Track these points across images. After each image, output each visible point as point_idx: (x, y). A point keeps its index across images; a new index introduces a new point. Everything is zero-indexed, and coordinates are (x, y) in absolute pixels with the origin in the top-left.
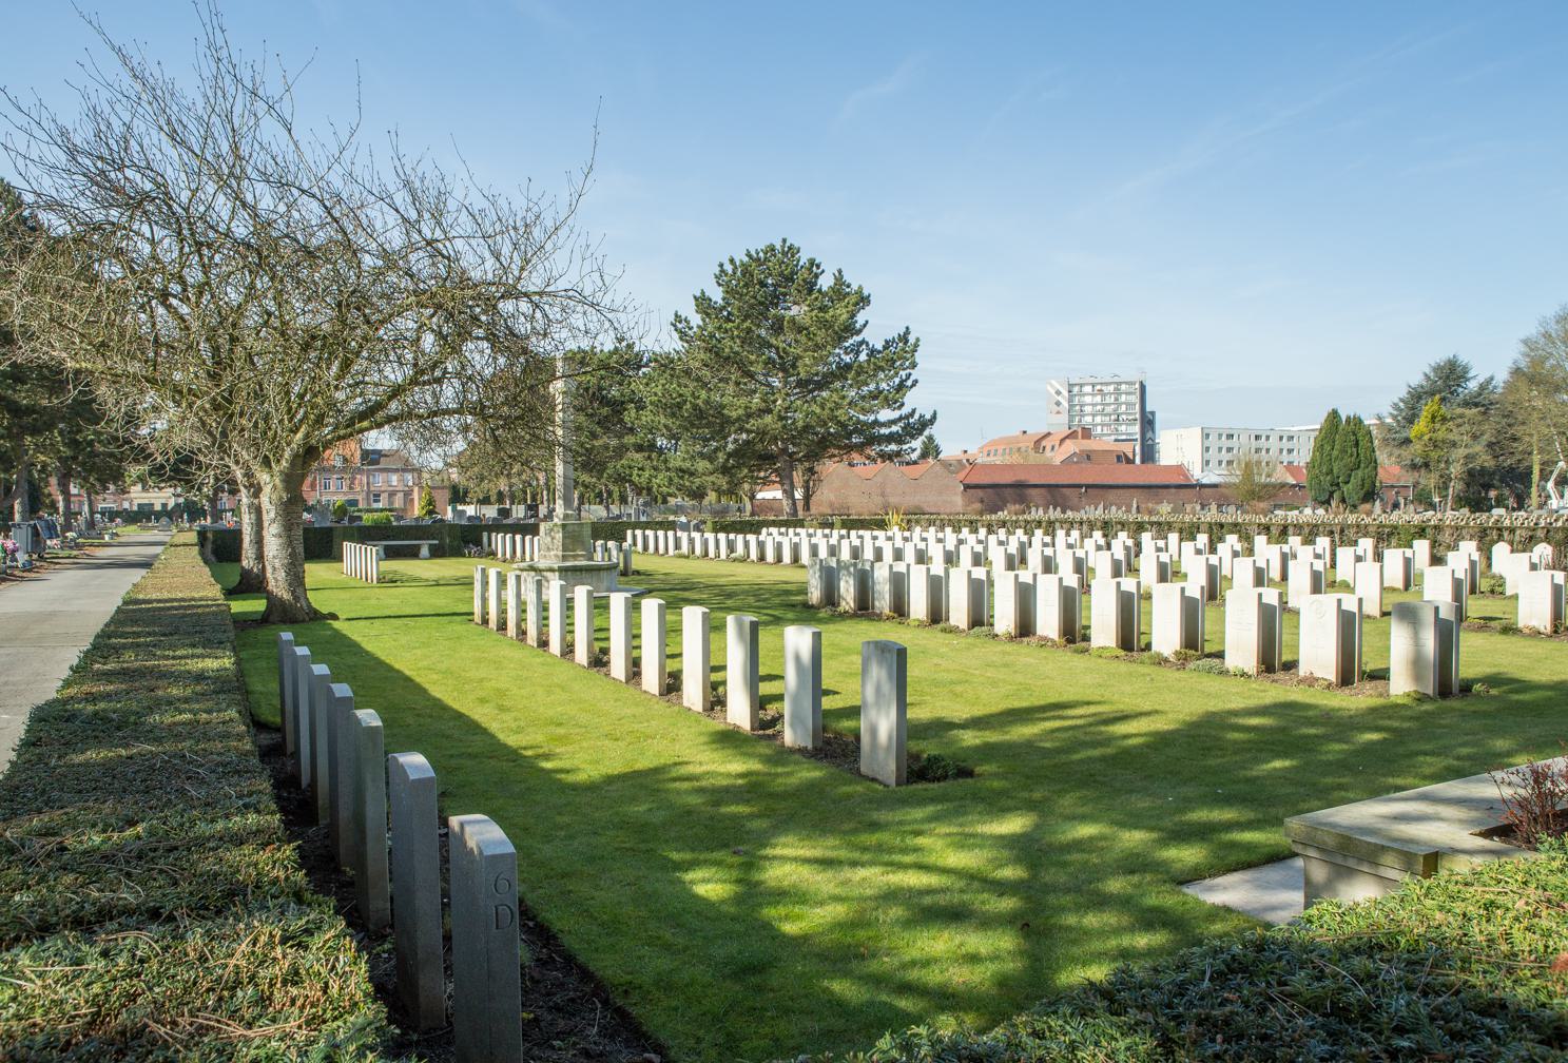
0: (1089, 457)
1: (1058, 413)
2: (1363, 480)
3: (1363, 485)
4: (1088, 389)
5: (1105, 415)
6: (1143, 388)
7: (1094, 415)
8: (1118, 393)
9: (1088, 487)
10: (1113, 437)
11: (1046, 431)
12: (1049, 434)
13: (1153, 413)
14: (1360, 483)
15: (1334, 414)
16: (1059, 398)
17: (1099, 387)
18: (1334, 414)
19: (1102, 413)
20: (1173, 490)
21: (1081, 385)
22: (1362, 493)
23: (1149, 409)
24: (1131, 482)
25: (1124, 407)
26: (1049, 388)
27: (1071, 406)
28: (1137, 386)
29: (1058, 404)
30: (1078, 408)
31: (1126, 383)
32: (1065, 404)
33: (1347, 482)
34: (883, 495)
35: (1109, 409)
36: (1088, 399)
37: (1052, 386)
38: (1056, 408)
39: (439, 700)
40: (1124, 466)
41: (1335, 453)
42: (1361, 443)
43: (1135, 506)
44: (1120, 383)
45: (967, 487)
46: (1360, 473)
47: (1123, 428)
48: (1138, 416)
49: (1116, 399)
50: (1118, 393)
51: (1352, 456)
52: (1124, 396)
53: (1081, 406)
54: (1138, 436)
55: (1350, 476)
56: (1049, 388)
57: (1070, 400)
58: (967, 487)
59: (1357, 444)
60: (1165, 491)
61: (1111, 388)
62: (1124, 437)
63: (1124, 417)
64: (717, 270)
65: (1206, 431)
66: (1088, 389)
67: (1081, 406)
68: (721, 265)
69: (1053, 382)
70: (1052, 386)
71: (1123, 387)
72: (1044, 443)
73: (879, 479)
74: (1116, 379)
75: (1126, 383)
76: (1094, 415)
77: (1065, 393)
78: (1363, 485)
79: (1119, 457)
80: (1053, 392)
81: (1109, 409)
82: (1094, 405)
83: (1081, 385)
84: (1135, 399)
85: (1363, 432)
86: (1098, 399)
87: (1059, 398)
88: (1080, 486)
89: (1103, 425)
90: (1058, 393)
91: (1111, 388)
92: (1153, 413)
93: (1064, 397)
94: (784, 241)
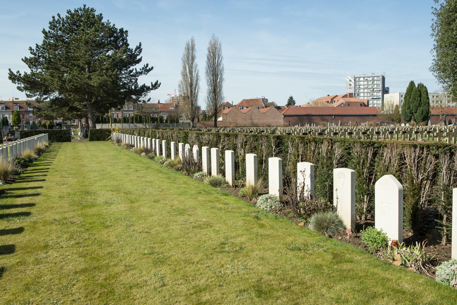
0: (349, 105)
1: (350, 88)
2: (422, 111)
3: (422, 113)
4: (362, 79)
5: (369, 89)
6: (383, 79)
7: (364, 89)
8: (373, 80)
9: (335, 116)
10: (371, 97)
11: (336, 95)
12: (337, 96)
13: (388, 88)
14: (421, 112)
15: (412, 83)
16: (351, 83)
17: (366, 78)
18: (412, 83)
19: (367, 88)
20: (371, 117)
21: (359, 78)
22: (422, 117)
23: (386, 86)
24: (353, 113)
25: (376, 86)
26: (347, 79)
27: (355, 86)
28: (381, 78)
29: (350, 85)
30: (358, 86)
31: (377, 77)
32: (353, 85)
33: (416, 113)
34: (251, 119)
35: (370, 87)
36: (362, 83)
37: (348, 78)
38: (349, 87)
39: (16, 208)
40: (363, 107)
41: (411, 100)
42: (422, 95)
43: (340, 123)
44: (374, 77)
45: (285, 116)
46: (421, 108)
47: (375, 94)
48: (381, 89)
49: (373, 83)
50: (373, 80)
51: (417, 101)
52: (376, 82)
53: (359, 86)
54: (381, 97)
55: (417, 110)
56: (347, 79)
57: (355, 84)
58: (285, 116)
59: (420, 96)
60: (368, 117)
61: (371, 79)
62: (375, 97)
63: (376, 89)
64: (51, 20)
65: (401, 94)
66: (362, 79)
67: (359, 86)
68: (54, 17)
69: (348, 77)
70: (348, 78)
71: (376, 78)
72: (335, 99)
73: (249, 113)
74: (373, 75)
75: (377, 77)
76: (364, 89)
77: (353, 81)
78: (422, 113)
79: (361, 105)
80: (348, 80)
81: (370, 87)
82: (364, 85)
83: (359, 78)
84: (380, 83)
85: (423, 90)
86: (366, 83)
87: (351, 83)
88: (332, 115)
89: (367, 93)
90: (350, 81)
91: (371, 79)
92: (388, 88)
93: (352, 83)
94: (85, 6)
